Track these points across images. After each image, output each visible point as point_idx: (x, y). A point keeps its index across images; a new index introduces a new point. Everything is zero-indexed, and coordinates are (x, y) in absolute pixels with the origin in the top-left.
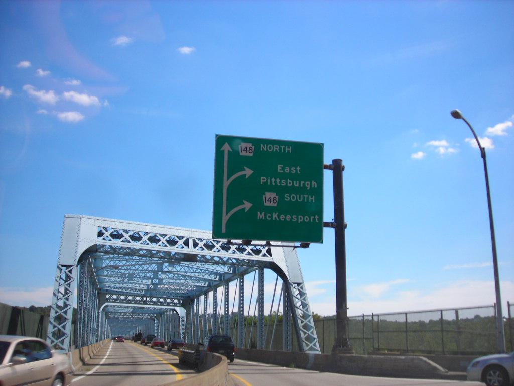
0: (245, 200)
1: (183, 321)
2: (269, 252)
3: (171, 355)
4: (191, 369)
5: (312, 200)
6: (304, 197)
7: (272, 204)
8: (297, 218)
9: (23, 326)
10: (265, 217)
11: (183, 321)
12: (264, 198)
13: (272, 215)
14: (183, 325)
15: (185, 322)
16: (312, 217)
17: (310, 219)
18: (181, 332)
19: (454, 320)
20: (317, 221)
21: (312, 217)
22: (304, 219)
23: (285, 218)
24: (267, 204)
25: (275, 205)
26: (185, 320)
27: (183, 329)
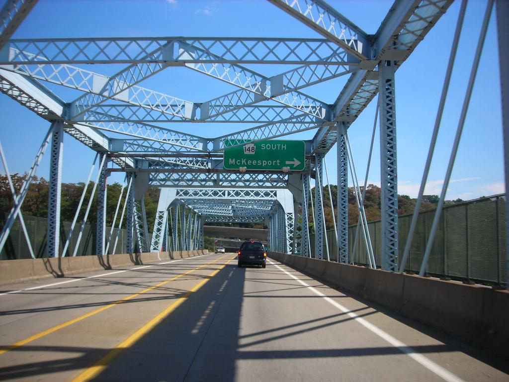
0: (296, 158)
1: (290, 219)
2: (275, 194)
3: (289, 268)
4: (327, 285)
5: (284, 148)
6: (277, 147)
7: (251, 153)
8: (262, 162)
9: (42, 249)
10: (236, 163)
11: (290, 219)
12: (244, 148)
13: (241, 161)
14: (291, 225)
15: (293, 220)
16: (274, 162)
17: (272, 164)
18: (288, 237)
19: (437, 197)
20: (112, 158)
21: (274, 162)
22: (267, 164)
23: (252, 163)
24: (247, 153)
25: (254, 153)
26: (293, 217)
27: (291, 232)
